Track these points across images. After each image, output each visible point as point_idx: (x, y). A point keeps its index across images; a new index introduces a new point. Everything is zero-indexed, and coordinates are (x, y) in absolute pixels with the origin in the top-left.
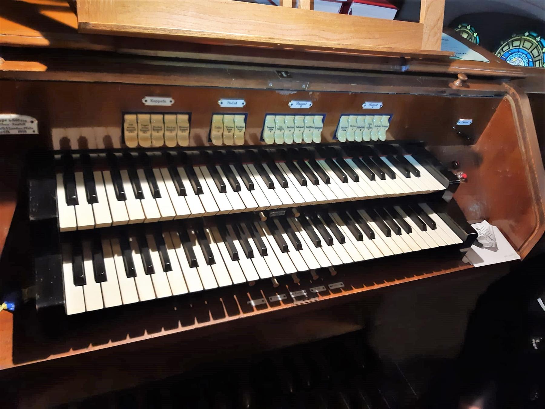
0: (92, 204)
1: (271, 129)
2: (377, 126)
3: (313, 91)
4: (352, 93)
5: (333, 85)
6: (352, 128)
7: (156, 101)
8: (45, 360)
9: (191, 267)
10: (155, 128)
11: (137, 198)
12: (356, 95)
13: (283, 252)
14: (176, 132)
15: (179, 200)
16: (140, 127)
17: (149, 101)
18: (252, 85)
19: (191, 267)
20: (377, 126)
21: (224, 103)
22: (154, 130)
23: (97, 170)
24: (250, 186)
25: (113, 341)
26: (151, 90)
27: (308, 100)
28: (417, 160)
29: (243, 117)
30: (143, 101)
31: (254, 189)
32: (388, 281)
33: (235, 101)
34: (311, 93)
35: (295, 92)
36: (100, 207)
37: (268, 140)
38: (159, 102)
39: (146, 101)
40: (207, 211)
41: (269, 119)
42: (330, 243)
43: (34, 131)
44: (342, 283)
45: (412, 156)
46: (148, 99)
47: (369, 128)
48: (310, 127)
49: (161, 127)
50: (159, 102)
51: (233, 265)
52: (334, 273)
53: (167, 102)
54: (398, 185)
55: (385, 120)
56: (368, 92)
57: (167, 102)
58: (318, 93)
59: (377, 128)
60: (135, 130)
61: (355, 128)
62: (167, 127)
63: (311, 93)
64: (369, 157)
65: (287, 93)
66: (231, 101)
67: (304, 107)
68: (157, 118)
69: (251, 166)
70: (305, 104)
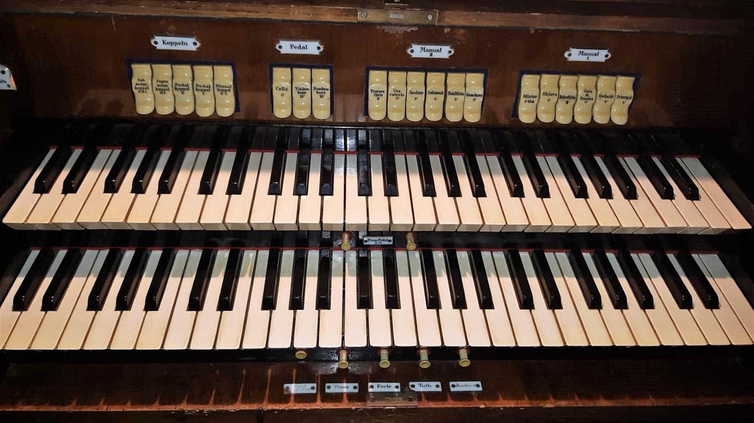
0: (300, 195)
1: (530, 99)
2: (605, 96)
3: (452, 27)
4: (537, 30)
5: (490, 15)
6: (547, 98)
7: (171, 44)
8: (145, 409)
9: (428, 308)
10: (178, 87)
11: (385, 196)
12: (545, 34)
13: (520, 309)
14: (211, 92)
15: (423, 203)
16: (155, 84)
17: (161, 43)
18: (329, 15)
19: (428, 308)
20: (605, 96)
21: (286, 47)
22: (176, 89)
23: (399, 152)
24: (542, 189)
25: (132, 404)
26: (165, 27)
27: (445, 43)
28: (165, 167)
29: (632, 79)
30: (409, 51)
31: (589, 198)
32: (581, 396)
33: (303, 44)
34: (447, 30)
35: (415, 29)
36: (400, 202)
37: (526, 116)
38: (176, 44)
39: (195, 44)
40: (509, 223)
41: (528, 83)
42: (620, 303)
43: (9, 86)
44: (479, 383)
45: (700, 160)
46: (158, 39)
47: (586, 99)
48: (457, 94)
49: (187, 85)
50: (176, 44)
51: (521, 316)
52: (464, 361)
53: (190, 44)
54: (645, 211)
55: (624, 84)
56: (573, 28)
57: (190, 44)
58: (462, 31)
59: (604, 99)
60: (147, 88)
61: (554, 99)
62: (197, 85)
63: (447, 30)
64: (586, 151)
65: (400, 30)
66: (296, 43)
67: (436, 55)
68: (585, 81)
69: (553, 160)
70: (439, 51)
